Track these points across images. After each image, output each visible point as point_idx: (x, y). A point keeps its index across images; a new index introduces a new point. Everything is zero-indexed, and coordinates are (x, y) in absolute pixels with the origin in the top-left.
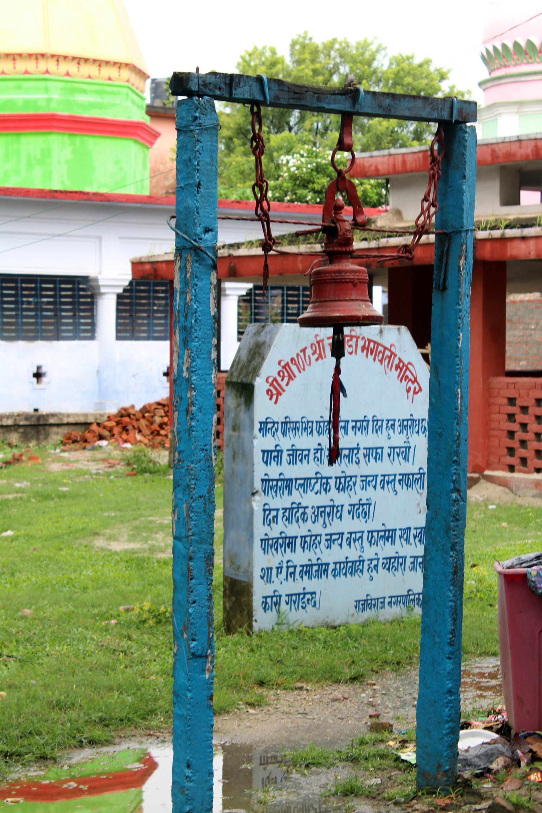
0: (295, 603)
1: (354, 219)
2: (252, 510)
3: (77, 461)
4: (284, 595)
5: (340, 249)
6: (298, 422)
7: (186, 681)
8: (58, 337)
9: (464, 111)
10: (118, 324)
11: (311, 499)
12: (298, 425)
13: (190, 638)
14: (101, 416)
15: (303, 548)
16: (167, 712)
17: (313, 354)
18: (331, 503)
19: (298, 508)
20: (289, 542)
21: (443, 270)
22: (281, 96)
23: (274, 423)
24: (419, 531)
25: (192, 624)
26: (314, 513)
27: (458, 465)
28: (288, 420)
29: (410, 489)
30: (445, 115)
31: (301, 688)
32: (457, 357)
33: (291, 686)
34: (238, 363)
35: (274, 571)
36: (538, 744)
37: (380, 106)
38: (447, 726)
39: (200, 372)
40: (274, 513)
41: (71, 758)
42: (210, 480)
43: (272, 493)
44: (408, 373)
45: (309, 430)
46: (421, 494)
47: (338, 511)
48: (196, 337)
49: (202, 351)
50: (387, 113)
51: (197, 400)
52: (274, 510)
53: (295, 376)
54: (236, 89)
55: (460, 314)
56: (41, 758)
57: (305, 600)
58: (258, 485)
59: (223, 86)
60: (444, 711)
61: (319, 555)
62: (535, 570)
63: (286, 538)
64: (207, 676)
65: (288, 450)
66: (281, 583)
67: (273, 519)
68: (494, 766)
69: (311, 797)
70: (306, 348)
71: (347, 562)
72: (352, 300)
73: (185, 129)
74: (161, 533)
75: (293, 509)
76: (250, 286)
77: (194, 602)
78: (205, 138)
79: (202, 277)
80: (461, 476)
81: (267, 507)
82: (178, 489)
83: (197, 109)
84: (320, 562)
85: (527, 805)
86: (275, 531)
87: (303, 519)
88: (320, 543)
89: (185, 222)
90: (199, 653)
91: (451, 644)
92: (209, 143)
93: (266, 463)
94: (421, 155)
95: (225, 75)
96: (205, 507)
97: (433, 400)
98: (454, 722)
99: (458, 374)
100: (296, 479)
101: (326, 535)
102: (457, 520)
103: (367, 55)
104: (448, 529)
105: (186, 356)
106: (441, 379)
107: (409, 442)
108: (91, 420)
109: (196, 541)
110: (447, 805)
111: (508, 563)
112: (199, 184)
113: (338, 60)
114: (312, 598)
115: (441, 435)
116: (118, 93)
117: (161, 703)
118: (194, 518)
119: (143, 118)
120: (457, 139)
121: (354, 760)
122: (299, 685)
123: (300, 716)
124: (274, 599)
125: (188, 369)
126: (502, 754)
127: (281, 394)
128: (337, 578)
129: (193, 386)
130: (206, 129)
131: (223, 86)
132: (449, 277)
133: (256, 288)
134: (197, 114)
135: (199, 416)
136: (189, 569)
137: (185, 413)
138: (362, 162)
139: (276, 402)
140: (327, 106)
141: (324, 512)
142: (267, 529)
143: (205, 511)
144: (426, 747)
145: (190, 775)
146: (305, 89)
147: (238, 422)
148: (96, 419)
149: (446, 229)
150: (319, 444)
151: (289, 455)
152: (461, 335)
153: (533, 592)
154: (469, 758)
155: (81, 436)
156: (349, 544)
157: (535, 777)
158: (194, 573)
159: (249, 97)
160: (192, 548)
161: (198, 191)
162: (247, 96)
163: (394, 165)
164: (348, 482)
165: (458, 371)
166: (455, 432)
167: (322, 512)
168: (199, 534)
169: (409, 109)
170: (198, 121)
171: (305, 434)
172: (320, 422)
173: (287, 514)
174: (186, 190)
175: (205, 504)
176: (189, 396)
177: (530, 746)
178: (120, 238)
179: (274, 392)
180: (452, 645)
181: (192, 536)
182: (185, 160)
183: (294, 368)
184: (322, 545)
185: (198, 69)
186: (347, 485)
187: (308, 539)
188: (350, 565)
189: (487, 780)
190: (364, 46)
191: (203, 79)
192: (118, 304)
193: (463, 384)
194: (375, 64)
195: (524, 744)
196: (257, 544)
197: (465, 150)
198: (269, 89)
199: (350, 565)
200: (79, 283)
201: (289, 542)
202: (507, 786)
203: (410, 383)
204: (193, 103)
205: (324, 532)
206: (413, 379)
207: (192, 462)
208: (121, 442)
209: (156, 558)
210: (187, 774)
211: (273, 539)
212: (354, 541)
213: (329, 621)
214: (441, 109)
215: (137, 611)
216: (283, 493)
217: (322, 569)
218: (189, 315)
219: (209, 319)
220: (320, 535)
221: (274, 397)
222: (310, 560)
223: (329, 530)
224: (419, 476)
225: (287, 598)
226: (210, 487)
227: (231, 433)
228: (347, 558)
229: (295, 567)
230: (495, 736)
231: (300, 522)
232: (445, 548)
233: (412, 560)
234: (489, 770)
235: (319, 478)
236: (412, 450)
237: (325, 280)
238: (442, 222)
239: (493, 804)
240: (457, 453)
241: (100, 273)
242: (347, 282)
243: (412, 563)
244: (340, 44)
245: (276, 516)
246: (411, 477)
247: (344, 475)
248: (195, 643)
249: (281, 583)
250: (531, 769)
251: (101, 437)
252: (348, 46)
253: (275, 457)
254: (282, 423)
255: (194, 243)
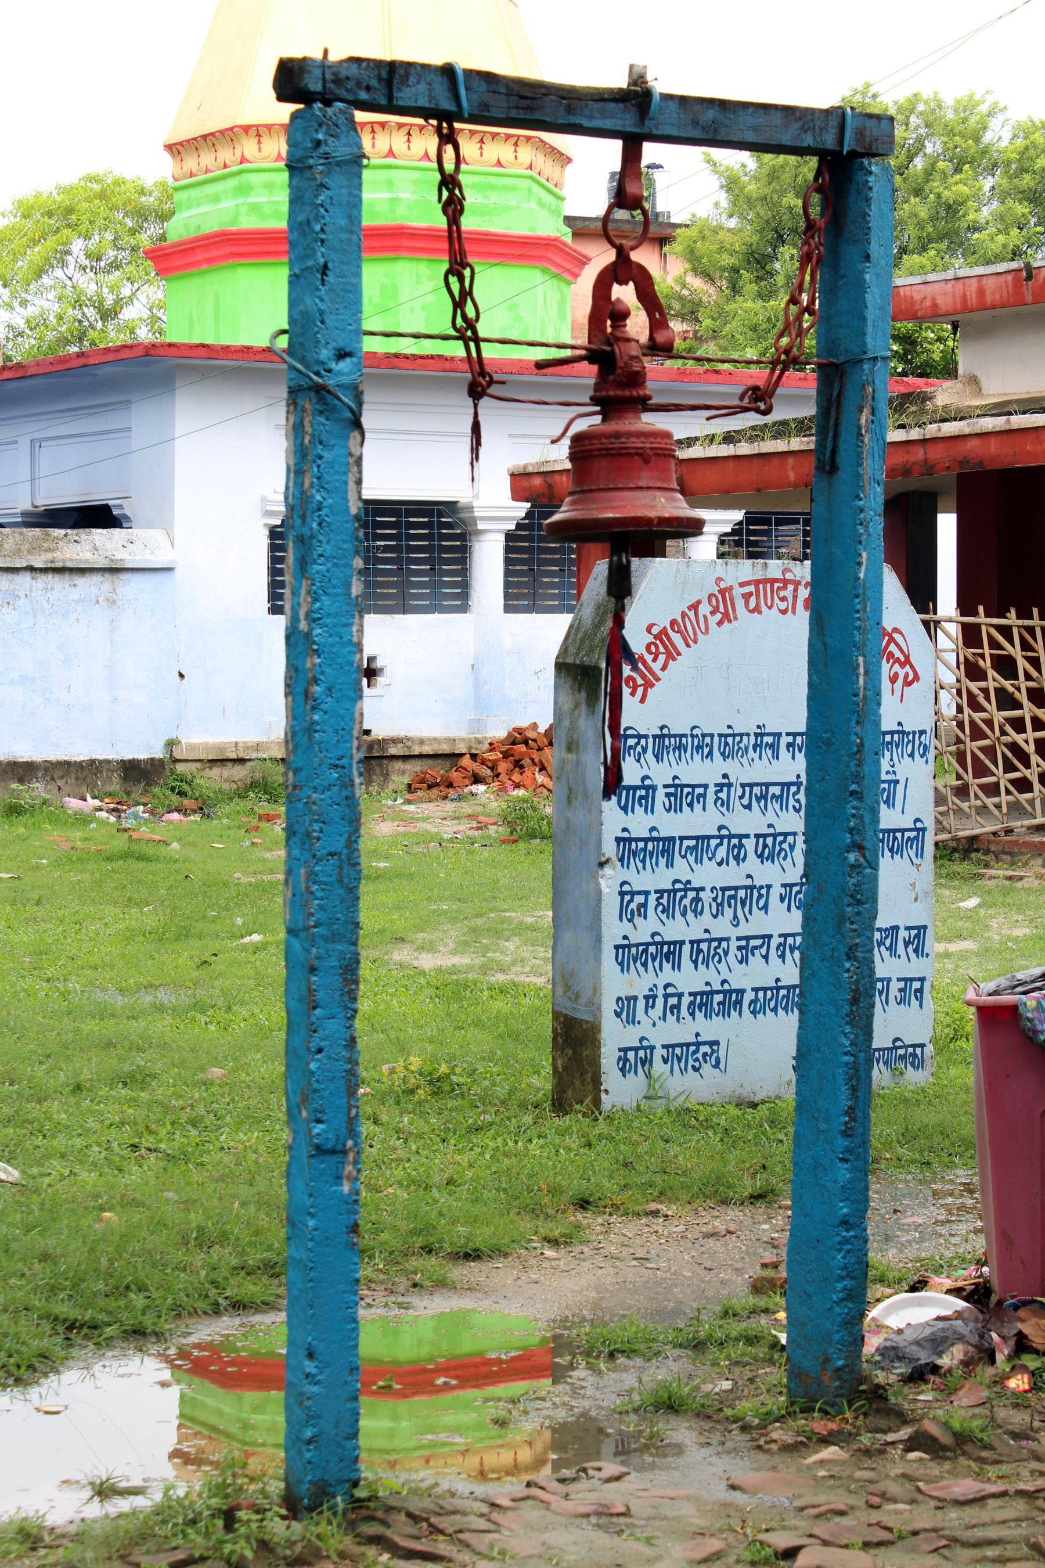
0: (679, 1060)
1: (651, 338)
2: (599, 892)
3: (425, 819)
4: (658, 1046)
5: (619, 393)
6: (685, 736)
7: (306, 1198)
8: (405, 609)
9: (867, 133)
10: (507, 585)
11: (709, 875)
12: (684, 740)
13: (313, 1117)
14: (479, 742)
15: (695, 962)
16: (391, 1253)
17: (712, 613)
18: (749, 882)
19: (686, 890)
20: (669, 952)
21: (831, 434)
22: (492, 103)
23: (639, 737)
24: (914, 932)
25: (315, 1091)
26: (715, 899)
27: (861, 799)
28: (665, 731)
29: (897, 857)
30: (829, 141)
31: (655, 1213)
32: (857, 597)
33: (636, 1209)
34: (578, 630)
35: (641, 1004)
36: (1034, 1320)
37: (696, 123)
38: (839, 1286)
39: (328, 621)
40: (639, 899)
41: (190, 1334)
42: (352, 821)
43: (635, 863)
44: (892, 647)
45: (706, 750)
46: (918, 866)
47: (760, 896)
48: (321, 555)
49: (334, 582)
50: (710, 137)
51: (322, 673)
52: (639, 893)
53: (679, 654)
54: (399, 89)
55: (862, 516)
56: (135, 1332)
57: (699, 1055)
58: (610, 849)
59: (374, 83)
60: (834, 1258)
61: (725, 975)
62: (1034, 998)
63: (662, 944)
64: (346, 1188)
65: (665, 786)
66: (654, 1025)
67: (639, 910)
68: (945, 1361)
69: (593, 1413)
70: (699, 602)
71: (778, 988)
72: (641, 488)
73: (301, 165)
74: (516, 939)
75: (675, 891)
76: (738, 515)
77: (320, 1051)
78: (336, 181)
79: (332, 442)
80: (867, 820)
81: (626, 888)
82: (295, 839)
83: (320, 126)
84: (726, 987)
85: (979, 1436)
86: (642, 931)
87: (695, 911)
88: (726, 953)
89: (301, 339)
90: (329, 1145)
91: (846, 1134)
92: (344, 191)
93: (625, 809)
94: (1010, 277)
95: (379, 64)
96: (340, 873)
97: (815, 678)
98: (853, 1278)
99: (858, 628)
100: (682, 838)
101: (739, 939)
102: (859, 902)
103: (972, 122)
104: (842, 919)
105: (303, 592)
106: (827, 639)
107: (894, 773)
108: (461, 748)
109: (322, 936)
110: (831, 1433)
111: (991, 986)
112: (325, 266)
113: (922, 131)
114: (713, 1051)
115: (828, 743)
116: (515, 189)
117: (384, 1237)
118: (319, 894)
119: (558, 230)
120: (854, 187)
121: (698, 1346)
122: (653, 1206)
123: (634, 1263)
124: (641, 1053)
125: (307, 615)
126: (961, 1338)
127: (652, 685)
128: (760, 1016)
129: (315, 647)
130: (339, 164)
131: (374, 83)
132: (842, 447)
133: (750, 519)
134: (320, 136)
135: (329, 703)
136: (309, 989)
137: (302, 697)
138: (908, 293)
139: (642, 700)
140: (586, 123)
141: (734, 897)
142: (626, 927)
143: (340, 881)
144: (803, 1324)
145: (314, 1371)
146: (543, 91)
147: (575, 737)
148: (470, 748)
149: (836, 357)
150: (725, 776)
151: (668, 795)
152: (864, 555)
153: (1030, 1039)
154: (901, 1345)
155: (442, 776)
156: (782, 957)
157: (1018, 1383)
158: (320, 995)
159: (427, 105)
160: (314, 950)
161: (323, 280)
162: (423, 102)
163: (964, 297)
164: (781, 843)
165: (858, 623)
166: (854, 738)
167: (730, 897)
168: (330, 924)
169: (755, 129)
170: (323, 149)
171: (697, 757)
172: (726, 736)
173: (664, 901)
174: (302, 280)
175: (341, 868)
176: (309, 665)
177: (1020, 1326)
178: (510, 436)
179: (640, 681)
180: (849, 1136)
181: (315, 927)
182: (301, 224)
183: (676, 638)
184: (731, 958)
185: (326, 52)
186: (778, 848)
187: (704, 946)
188: (783, 992)
189: (924, 1387)
190: (967, 107)
191: (334, 69)
192: (508, 549)
193: (868, 649)
194: (988, 138)
195: (1010, 1321)
196: (608, 954)
197: (869, 206)
198: (467, 89)
199: (783, 992)
200: (441, 514)
201: (669, 952)
202: (960, 1399)
203: (897, 665)
204: (314, 114)
205: (733, 933)
206: (903, 659)
207: (315, 789)
208: (510, 788)
209: (488, 982)
210: (308, 1370)
211: (637, 945)
212: (792, 951)
213: (745, 1094)
214: (821, 129)
215: (401, 1072)
216: (657, 864)
217: (731, 1000)
218: (308, 514)
219: (347, 522)
220: (728, 939)
221: (640, 690)
222: (707, 984)
223: (744, 930)
224: (913, 834)
225: (664, 1052)
226: (350, 837)
227: (565, 755)
228: (778, 980)
229: (680, 996)
230: (961, 1304)
231: (690, 915)
232: (836, 954)
233: (902, 984)
234: (935, 1369)
235: (723, 835)
236: (900, 788)
237: (590, 451)
238: (828, 344)
239: (917, 1432)
240: (858, 778)
241: (476, 496)
242: (631, 455)
243: (900, 990)
244: (926, 103)
245: (644, 905)
246: (899, 835)
247: (771, 831)
248: (321, 1126)
249: (654, 1025)
250: (1013, 1368)
251: (477, 780)
252: (940, 107)
253: (641, 797)
254: (655, 737)
255: (315, 378)
